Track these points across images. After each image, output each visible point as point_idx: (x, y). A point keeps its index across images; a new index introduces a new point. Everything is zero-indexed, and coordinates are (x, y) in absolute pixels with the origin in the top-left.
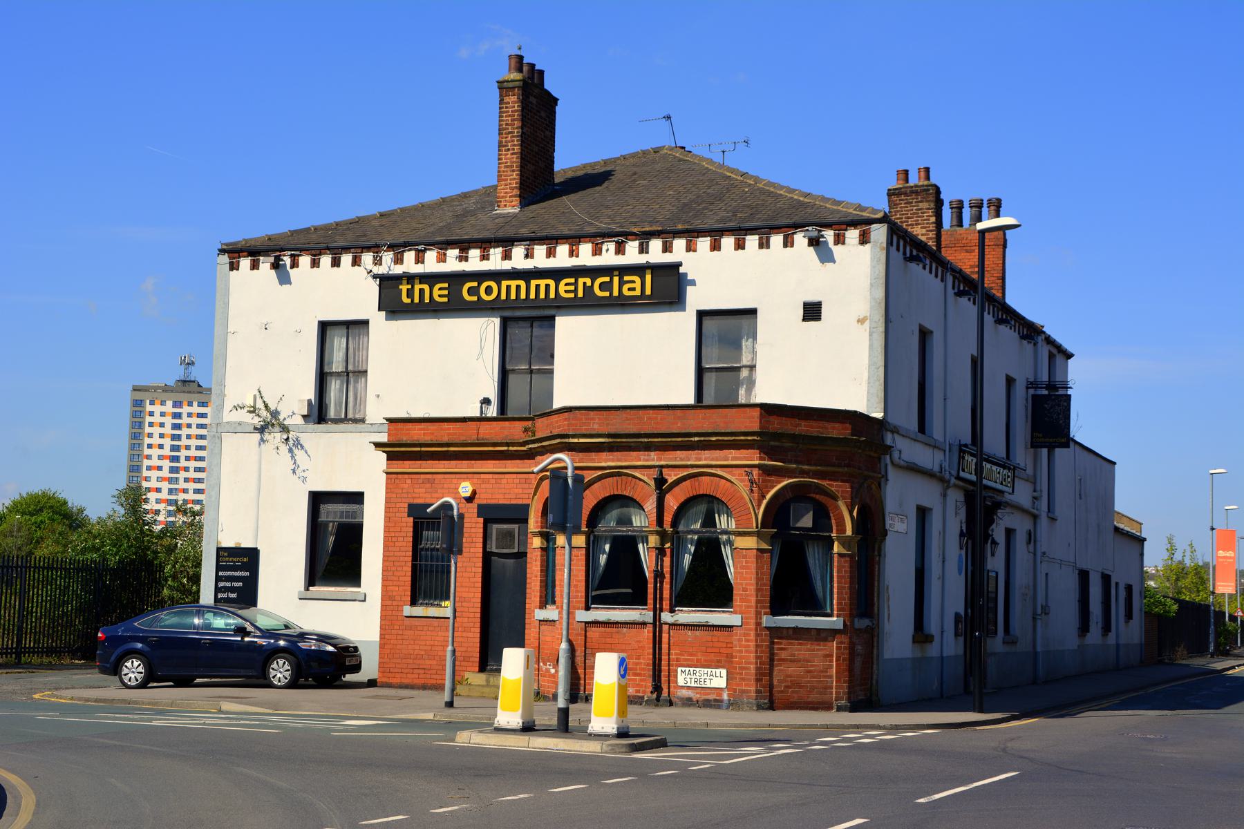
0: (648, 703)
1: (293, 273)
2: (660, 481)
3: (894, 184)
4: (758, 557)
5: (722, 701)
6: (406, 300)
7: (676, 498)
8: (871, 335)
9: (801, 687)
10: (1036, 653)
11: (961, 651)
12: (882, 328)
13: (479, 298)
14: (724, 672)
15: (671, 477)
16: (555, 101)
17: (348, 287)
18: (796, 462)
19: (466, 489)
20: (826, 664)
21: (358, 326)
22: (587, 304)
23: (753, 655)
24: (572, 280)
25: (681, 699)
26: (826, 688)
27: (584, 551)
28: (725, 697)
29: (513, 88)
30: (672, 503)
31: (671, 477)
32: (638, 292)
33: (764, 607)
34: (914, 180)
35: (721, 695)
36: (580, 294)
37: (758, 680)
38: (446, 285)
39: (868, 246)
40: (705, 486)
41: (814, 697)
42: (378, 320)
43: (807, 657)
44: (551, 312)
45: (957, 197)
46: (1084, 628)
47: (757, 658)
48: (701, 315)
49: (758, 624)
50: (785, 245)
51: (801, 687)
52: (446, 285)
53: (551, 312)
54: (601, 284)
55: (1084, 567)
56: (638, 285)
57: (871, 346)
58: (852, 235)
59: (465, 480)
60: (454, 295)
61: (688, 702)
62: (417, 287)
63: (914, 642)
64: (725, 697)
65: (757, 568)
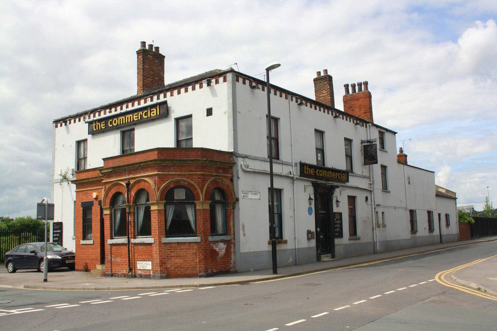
0: (125, 276)
1: (70, 126)
2: (128, 185)
3: (316, 76)
4: (158, 213)
5: (150, 275)
6: (95, 130)
7: (134, 192)
8: (228, 118)
9: (182, 268)
10: (296, 249)
11: (271, 249)
12: (232, 115)
13: (113, 125)
14: (150, 263)
15: (132, 182)
16: (162, 58)
17: (80, 129)
18: (175, 171)
19: (94, 195)
20: (193, 258)
21: (85, 141)
22: (142, 122)
23: (158, 255)
24: (137, 114)
25: (139, 274)
26: (194, 267)
27: (109, 216)
28: (152, 274)
29: (140, 53)
30: (133, 193)
31: (132, 182)
32: (155, 114)
33: (163, 234)
34: (322, 74)
35: (150, 272)
36: (139, 119)
37: (161, 266)
38: (104, 122)
39: (226, 83)
40: (142, 185)
41: (189, 272)
42: (89, 137)
43: (185, 255)
44: (132, 127)
45: (352, 83)
46: (414, 230)
47: (160, 256)
48: (178, 120)
49: (160, 242)
50: (200, 88)
51: (182, 268)
52: (104, 122)
53: (132, 127)
54: (145, 113)
55: (413, 208)
56: (155, 112)
57: (229, 122)
58: (221, 79)
59: (94, 192)
60: (103, 126)
61: (141, 276)
62: (97, 124)
63: (411, 234)
64: (152, 274)
65: (158, 218)
